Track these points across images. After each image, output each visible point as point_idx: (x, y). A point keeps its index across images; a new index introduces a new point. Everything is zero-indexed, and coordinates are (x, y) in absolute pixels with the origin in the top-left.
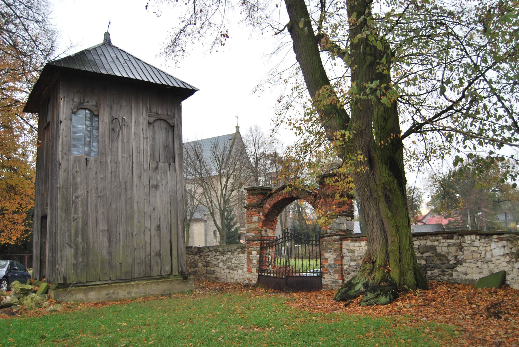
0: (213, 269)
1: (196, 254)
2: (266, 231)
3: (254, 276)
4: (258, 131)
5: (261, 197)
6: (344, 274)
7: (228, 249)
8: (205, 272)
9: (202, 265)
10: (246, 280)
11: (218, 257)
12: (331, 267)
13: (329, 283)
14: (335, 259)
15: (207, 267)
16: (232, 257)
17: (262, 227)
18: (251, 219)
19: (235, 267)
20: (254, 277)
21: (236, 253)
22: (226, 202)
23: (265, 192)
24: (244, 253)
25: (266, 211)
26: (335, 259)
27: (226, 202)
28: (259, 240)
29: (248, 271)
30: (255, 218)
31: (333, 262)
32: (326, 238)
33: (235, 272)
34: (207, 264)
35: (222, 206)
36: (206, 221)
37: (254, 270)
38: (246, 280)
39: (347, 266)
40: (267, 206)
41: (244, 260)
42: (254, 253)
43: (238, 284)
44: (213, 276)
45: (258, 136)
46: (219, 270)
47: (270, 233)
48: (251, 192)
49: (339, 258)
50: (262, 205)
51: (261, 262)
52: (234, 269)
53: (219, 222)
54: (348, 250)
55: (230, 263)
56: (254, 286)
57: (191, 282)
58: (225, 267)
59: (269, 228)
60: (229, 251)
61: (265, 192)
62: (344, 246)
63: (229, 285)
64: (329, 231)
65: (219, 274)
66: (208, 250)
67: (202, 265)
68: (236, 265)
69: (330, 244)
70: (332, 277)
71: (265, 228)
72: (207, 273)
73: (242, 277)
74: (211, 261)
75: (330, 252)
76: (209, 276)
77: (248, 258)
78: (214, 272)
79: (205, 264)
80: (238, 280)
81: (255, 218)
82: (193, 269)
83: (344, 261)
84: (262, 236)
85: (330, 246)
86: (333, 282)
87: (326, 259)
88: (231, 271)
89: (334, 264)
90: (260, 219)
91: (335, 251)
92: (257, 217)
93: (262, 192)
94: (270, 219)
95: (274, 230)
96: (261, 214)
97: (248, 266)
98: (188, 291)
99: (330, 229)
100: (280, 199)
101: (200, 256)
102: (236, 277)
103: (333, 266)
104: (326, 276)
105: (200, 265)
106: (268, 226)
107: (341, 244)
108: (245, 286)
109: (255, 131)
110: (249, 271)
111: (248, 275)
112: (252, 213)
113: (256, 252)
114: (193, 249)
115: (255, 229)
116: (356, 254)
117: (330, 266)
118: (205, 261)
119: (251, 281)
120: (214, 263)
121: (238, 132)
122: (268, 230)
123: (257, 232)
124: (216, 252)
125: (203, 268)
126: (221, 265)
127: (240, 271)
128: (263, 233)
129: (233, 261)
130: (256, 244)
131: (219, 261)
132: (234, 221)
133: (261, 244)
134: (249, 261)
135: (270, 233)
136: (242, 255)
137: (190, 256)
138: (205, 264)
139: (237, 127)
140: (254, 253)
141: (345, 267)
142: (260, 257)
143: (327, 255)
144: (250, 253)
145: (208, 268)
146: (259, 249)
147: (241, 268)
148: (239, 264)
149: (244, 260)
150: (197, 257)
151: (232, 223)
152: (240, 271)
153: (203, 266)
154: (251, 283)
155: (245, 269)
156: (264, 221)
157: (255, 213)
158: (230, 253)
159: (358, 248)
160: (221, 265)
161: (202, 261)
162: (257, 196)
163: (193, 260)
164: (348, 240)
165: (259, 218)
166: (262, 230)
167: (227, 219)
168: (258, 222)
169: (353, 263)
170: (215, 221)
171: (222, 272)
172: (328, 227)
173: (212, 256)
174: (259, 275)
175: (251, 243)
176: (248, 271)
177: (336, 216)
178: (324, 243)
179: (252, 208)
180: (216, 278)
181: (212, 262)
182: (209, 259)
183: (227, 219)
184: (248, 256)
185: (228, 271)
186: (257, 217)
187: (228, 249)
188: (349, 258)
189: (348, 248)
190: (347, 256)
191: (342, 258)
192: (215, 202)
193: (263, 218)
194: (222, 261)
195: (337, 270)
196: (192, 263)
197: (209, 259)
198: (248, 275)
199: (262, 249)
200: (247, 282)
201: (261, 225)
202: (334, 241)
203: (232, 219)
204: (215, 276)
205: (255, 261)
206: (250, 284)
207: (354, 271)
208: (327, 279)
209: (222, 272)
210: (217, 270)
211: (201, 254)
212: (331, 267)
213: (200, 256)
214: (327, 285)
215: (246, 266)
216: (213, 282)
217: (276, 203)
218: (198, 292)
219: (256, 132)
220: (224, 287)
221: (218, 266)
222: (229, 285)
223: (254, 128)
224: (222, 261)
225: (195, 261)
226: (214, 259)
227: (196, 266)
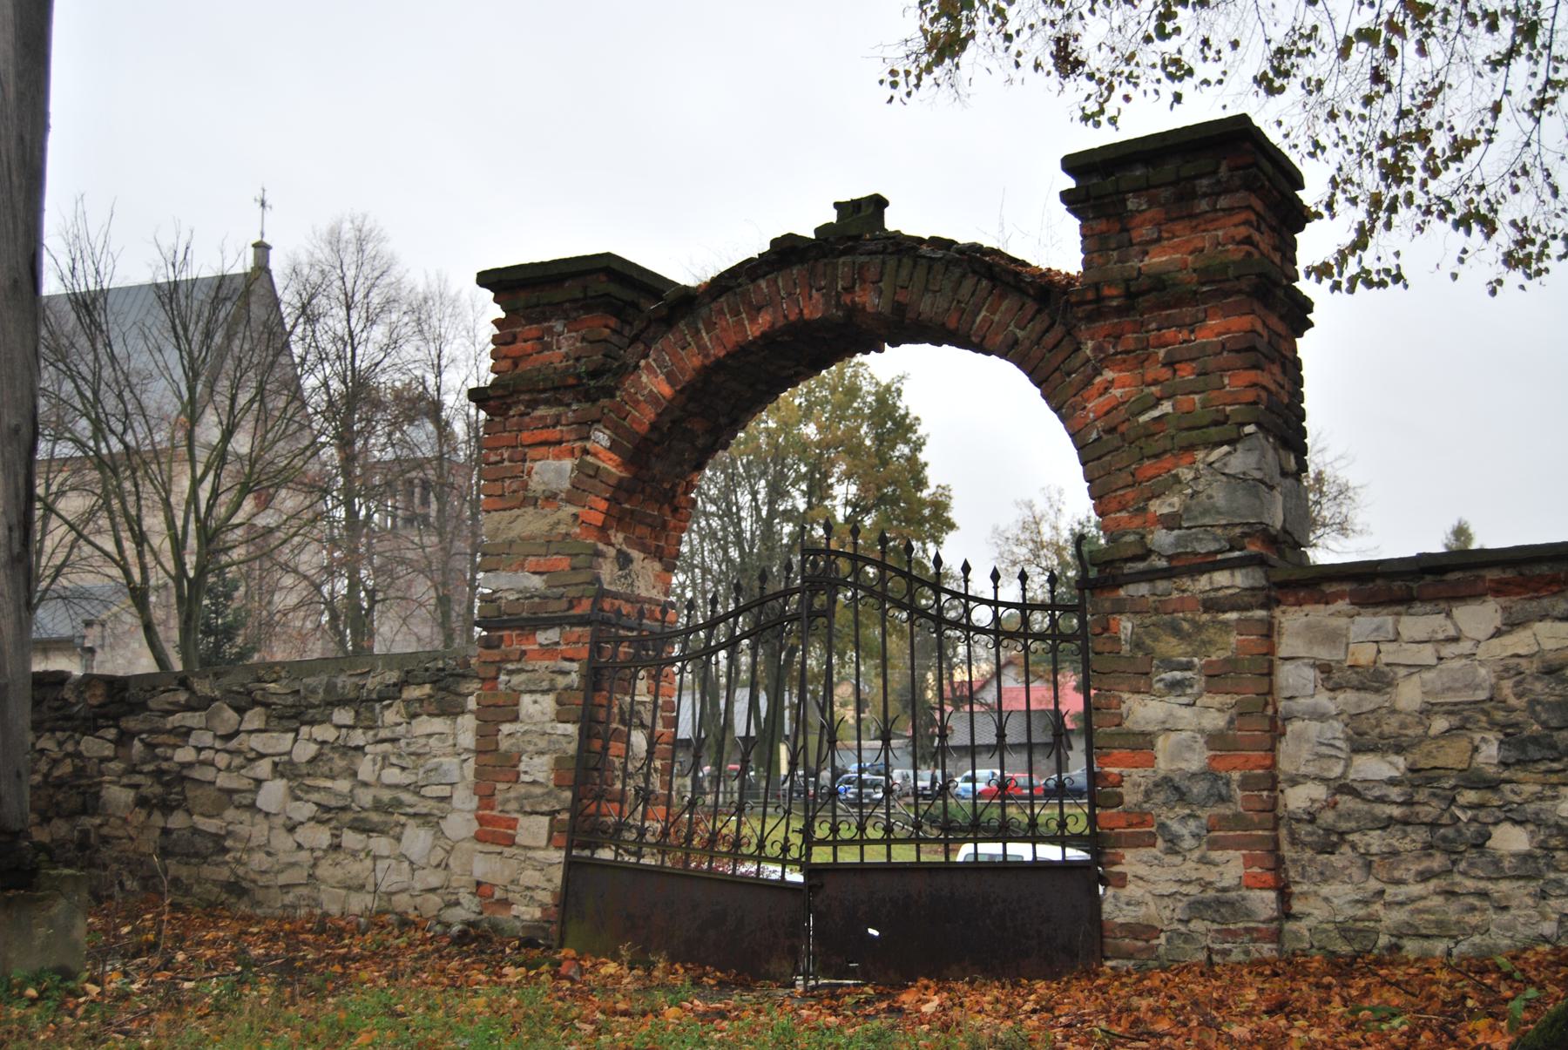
0: (211, 825)
1: (90, 725)
2: (624, 560)
3: (534, 872)
4: (369, 248)
5: (601, 325)
6: (1287, 851)
7: (331, 688)
8: (148, 843)
9: (127, 796)
10: (465, 897)
11: (257, 742)
12: (1181, 795)
13: (1150, 911)
14: (1215, 740)
15: (167, 808)
16: (358, 738)
17: (603, 531)
18: (522, 478)
19: (378, 806)
20: (530, 877)
21: (390, 716)
22: (210, 538)
23: (628, 295)
24: (450, 711)
25: (644, 417)
26: (1215, 740)
27: (210, 538)
28: (582, 621)
29: (479, 838)
30: (552, 472)
31: (1196, 761)
32: (1143, 589)
33: (381, 844)
34: (172, 790)
35: (190, 560)
36: (91, 651)
37: (534, 829)
38: (465, 897)
39: (1319, 792)
40: (653, 382)
41: (450, 763)
42: (537, 708)
43: (404, 923)
44: (207, 871)
45: (366, 269)
46: (258, 831)
47: (645, 580)
48: (523, 297)
49: (1255, 729)
50: (607, 381)
51: (586, 771)
52: (380, 819)
53: (170, 634)
54: (1325, 669)
55: (343, 785)
56: (528, 943)
57: (59, 907)
58: (305, 810)
59: (643, 548)
60: (343, 703)
61: (628, 295)
62: (1287, 645)
63: (339, 934)
64: (1162, 538)
65: (258, 860)
66: (182, 697)
67: (127, 796)
68: (386, 796)
69: (1176, 630)
70: (1190, 869)
71: (618, 538)
72: (165, 853)
73: (434, 879)
74: (197, 774)
75: (1174, 686)
76: (184, 872)
77: (486, 746)
78: (219, 843)
79: (152, 789)
80: (402, 902)
81: (552, 472)
82: (61, 828)
83: (1293, 755)
84: (602, 594)
85: (1170, 646)
86: (1198, 908)
87: (1142, 743)
88: (350, 839)
89: (1209, 774)
90: (587, 475)
91: (1216, 678)
92: (568, 464)
93: (613, 288)
94: (650, 494)
95: (669, 561)
96: (601, 438)
97: (486, 798)
98: (36, 980)
99: (1171, 522)
100: (753, 331)
101: (124, 739)
102: (392, 877)
103: (1198, 788)
104: (1131, 862)
105: (118, 796)
106: (642, 530)
107: (1269, 632)
108: (462, 939)
109: (352, 248)
110: (495, 833)
111: (486, 866)
112: (526, 437)
113: (548, 703)
114: (69, 695)
115: (550, 543)
116: (1409, 695)
117: (1174, 789)
118: (158, 774)
119: (506, 903)
120: (223, 781)
121: (262, 268)
122: (636, 554)
123: (564, 563)
124: (241, 711)
125: (141, 815)
126: (273, 794)
127: (417, 840)
128: (607, 572)
129: (366, 769)
130: (548, 650)
131: (264, 768)
132: (239, 640)
133: (596, 648)
134: (495, 765)
135: (645, 580)
136: (438, 725)
137: (47, 743)
138: (152, 789)
139: (262, 248)
140: (537, 708)
141: (1297, 798)
142: (585, 735)
143: (1143, 711)
144: (500, 711)
145: (177, 821)
146: (574, 679)
147: (424, 819)
148: (416, 788)
149: (450, 763)
150: (92, 746)
151: (229, 650)
152: (417, 840)
153: (142, 802)
154: (502, 916)
155: (461, 823)
156: (620, 492)
157: (554, 434)
158: (344, 716)
159: (1427, 654)
160: (273, 794)
161: (133, 770)
162: (571, 323)
163: (66, 768)
164: (1327, 600)
165: (580, 468)
166: (599, 554)
167: (209, 630)
168: (576, 494)
169: (1373, 768)
170: (149, 628)
171: (283, 842)
172: (1159, 507)
173: (207, 738)
174: (571, 865)
175: (513, 641)
176: (479, 838)
177: (1228, 431)
178: (1126, 626)
179: (533, 404)
180: (236, 888)
181: (207, 774)
182: (184, 755)
183: (209, 630)
184: (487, 736)
185: (323, 837)
186: (568, 464)
187: (331, 688)
188: (1336, 729)
189: (1323, 654)
190: (1321, 717)
191: (1276, 730)
192: (156, 541)
193: (611, 465)
194: (285, 768)
195: (1237, 821)
196: (60, 784)
197: (184, 755)
198: (486, 866)
199: (596, 676)
200: (467, 909)
201: (598, 519)
202: (1212, 605)
203: (228, 632)
204: (224, 874)
205: (538, 768)
206: (496, 928)
207: (1388, 823)
208: (1144, 890)
209: (283, 842)
210: (242, 830)
211: (131, 723)
212: (1181, 795)
213: (124, 739)
214: (1144, 931)
215: (465, 800)
216: (212, 911)
217: (719, 365)
218: (115, 982)
219: (361, 250)
220: (316, 952)
221: (252, 807)
222: (339, 934)
223: (348, 233)
224: (285, 768)
225: (79, 772)
226: (222, 760)
227: (91, 802)
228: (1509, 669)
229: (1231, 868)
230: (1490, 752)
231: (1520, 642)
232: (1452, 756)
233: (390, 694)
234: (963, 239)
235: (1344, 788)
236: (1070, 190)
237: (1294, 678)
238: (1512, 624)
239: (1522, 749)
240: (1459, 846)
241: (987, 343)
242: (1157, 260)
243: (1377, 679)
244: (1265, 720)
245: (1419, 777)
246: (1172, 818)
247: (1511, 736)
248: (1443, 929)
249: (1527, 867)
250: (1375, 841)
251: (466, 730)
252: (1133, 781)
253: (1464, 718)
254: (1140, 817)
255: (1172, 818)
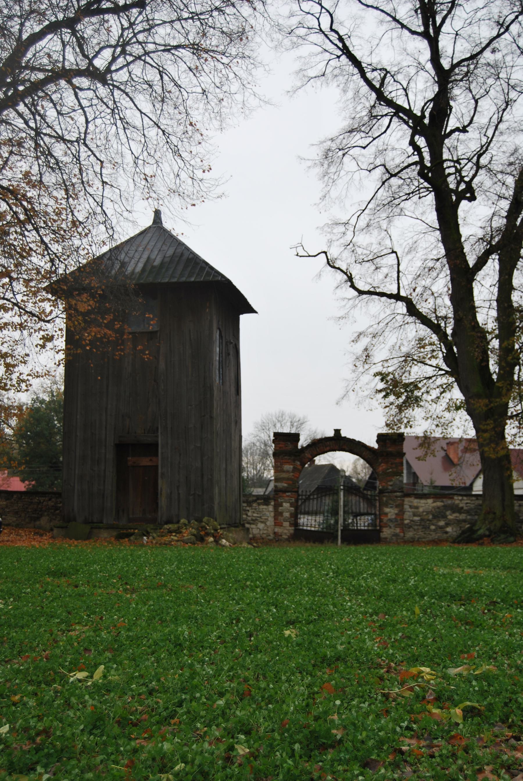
20: (286, 531)
26: (396, 514)
31: (394, 517)
41: (267, 513)
42: (286, 505)
62: (405, 503)
64: (390, 488)
85: (391, 502)
86: (394, 535)
91: (397, 506)
104: (384, 529)
107: (403, 501)
110: (277, 524)
113: (288, 504)
115: (288, 479)
117: (390, 520)
129: (250, 514)
136: (265, 507)
140: (286, 505)
143: (387, 510)
147: (262, 522)
148: (260, 517)
149: (267, 513)
152: (261, 526)
175: (281, 494)
178: (385, 499)
202: (397, 497)
205: (287, 515)
214: (386, 538)
228: (433, 507)
229: (398, 530)
230: (431, 517)
231: (435, 504)
232: (426, 517)
233: (255, 501)
234: (357, 439)
235: (412, 521)
236: (298, 440)
237: (406, 507)
238: (434, 502)
239: (435, 517)
240: (426, 528)
241: (498, 429)
242: (390, 449)
243: (417, 508)
244: (402, 512)
245: (422, 520)
246: (391, 524)
247: (433, 515)
248: (424, 538)
249: (434, 531)
250: (416, 527)
251: (271, 508)
252: (385, 519)
253: (428, 513)
254: (386, 524)
255: (391, 524)
